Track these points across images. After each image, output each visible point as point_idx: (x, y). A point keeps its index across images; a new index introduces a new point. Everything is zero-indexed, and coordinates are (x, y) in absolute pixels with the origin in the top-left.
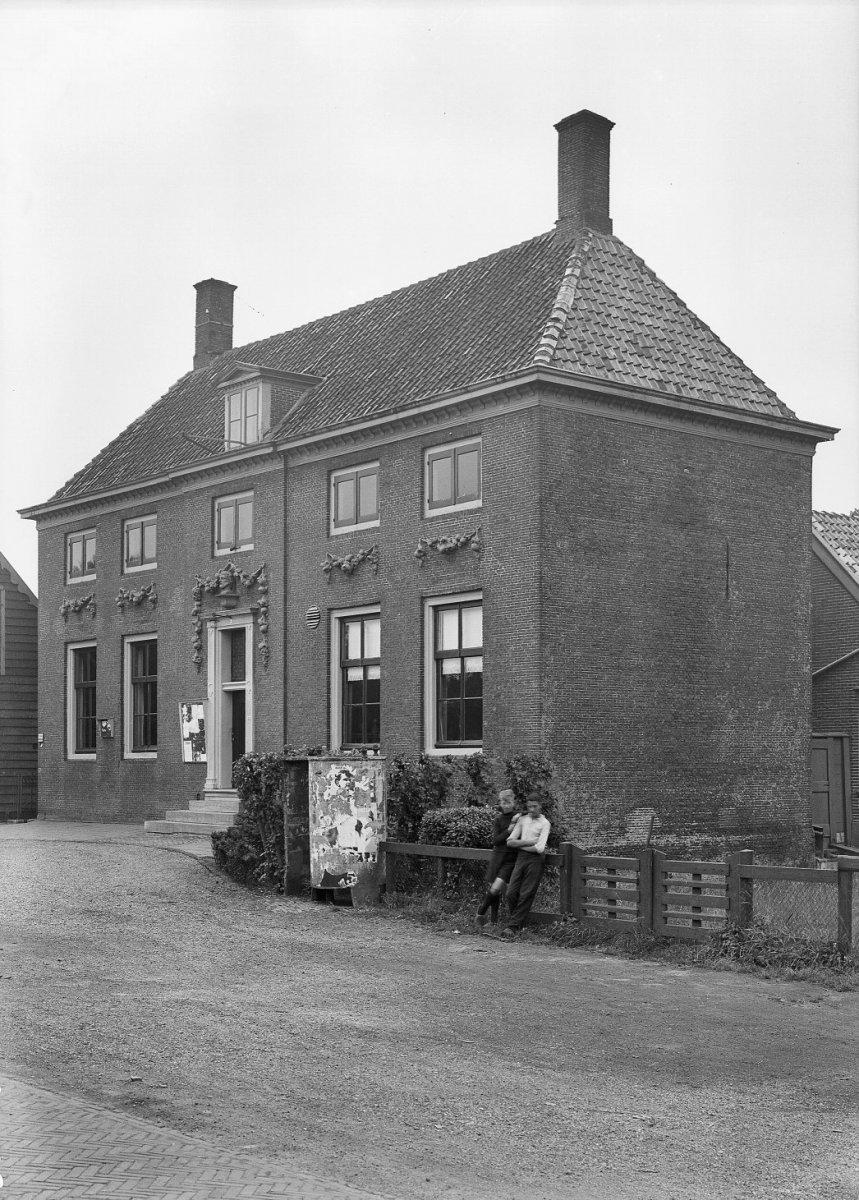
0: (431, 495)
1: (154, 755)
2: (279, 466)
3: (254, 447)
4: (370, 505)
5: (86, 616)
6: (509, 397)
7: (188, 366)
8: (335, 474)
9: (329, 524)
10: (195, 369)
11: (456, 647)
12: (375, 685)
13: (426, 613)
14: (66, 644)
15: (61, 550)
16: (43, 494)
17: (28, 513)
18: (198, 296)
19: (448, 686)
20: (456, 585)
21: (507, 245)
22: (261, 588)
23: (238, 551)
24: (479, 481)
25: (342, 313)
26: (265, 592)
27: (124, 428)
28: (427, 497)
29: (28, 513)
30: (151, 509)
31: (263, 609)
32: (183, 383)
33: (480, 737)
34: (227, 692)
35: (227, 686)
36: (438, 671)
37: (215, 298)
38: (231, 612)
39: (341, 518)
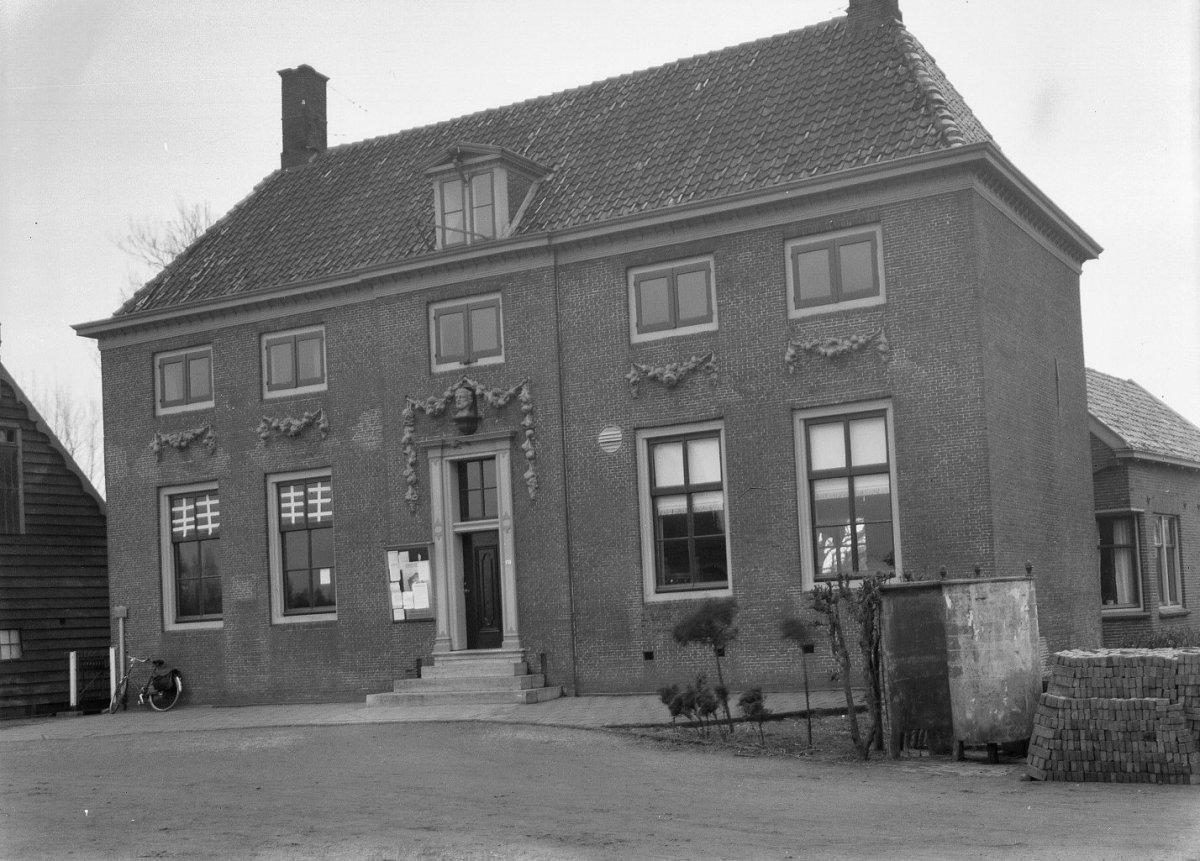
0: (270, 378)
1: (219, 625)
2: (548, 262)
3: (502, 243)
5: (197, 453)
6: (776, 209)
7: (276, 164)
8: (159, 358)
11: (681, 482)
12: (710, 520)
13: (269, 488)
16: (105, 308)
17: (84, 330)
18: (283, 83)
19: (669, 526)
20: (849, 394)
21: (813, 22)
22: (525, 407)
23: (474, 365)
25: (528, 103)
26: (531, 412)
28: (265, 379)
30: (316, 319)
31: (529, 432)
34: (458, 535)
36: (654, 514)
37: (304, 92)
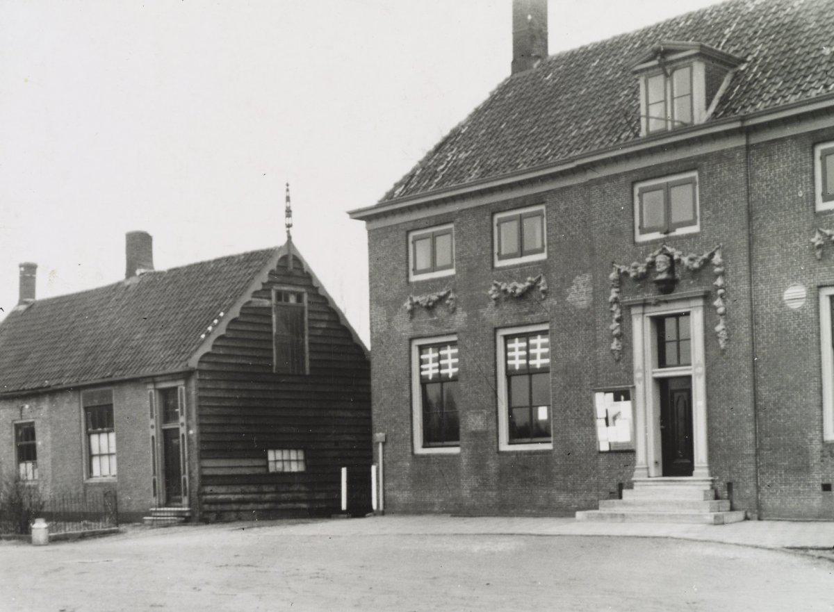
2: (741, 142)
4: (444, 256)
5: (441, 312)
7: (507, 72)
9: (634, 231)
10: (513, 72)
14: (411, 340)
15: (403, 248)
16: (371, 197)
17: (356, 215)
24: (452, 257)
26: (723, 274)
27: (446, 132)
29: (356, 215)
30: (538, 200)
31: (720, 291)
32: (504, 88)
33: (457, 439)
35: (656, 372)
38: (668, 297)
39: (503, 253)
